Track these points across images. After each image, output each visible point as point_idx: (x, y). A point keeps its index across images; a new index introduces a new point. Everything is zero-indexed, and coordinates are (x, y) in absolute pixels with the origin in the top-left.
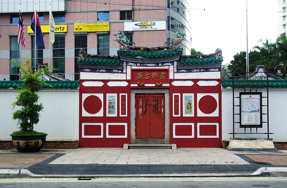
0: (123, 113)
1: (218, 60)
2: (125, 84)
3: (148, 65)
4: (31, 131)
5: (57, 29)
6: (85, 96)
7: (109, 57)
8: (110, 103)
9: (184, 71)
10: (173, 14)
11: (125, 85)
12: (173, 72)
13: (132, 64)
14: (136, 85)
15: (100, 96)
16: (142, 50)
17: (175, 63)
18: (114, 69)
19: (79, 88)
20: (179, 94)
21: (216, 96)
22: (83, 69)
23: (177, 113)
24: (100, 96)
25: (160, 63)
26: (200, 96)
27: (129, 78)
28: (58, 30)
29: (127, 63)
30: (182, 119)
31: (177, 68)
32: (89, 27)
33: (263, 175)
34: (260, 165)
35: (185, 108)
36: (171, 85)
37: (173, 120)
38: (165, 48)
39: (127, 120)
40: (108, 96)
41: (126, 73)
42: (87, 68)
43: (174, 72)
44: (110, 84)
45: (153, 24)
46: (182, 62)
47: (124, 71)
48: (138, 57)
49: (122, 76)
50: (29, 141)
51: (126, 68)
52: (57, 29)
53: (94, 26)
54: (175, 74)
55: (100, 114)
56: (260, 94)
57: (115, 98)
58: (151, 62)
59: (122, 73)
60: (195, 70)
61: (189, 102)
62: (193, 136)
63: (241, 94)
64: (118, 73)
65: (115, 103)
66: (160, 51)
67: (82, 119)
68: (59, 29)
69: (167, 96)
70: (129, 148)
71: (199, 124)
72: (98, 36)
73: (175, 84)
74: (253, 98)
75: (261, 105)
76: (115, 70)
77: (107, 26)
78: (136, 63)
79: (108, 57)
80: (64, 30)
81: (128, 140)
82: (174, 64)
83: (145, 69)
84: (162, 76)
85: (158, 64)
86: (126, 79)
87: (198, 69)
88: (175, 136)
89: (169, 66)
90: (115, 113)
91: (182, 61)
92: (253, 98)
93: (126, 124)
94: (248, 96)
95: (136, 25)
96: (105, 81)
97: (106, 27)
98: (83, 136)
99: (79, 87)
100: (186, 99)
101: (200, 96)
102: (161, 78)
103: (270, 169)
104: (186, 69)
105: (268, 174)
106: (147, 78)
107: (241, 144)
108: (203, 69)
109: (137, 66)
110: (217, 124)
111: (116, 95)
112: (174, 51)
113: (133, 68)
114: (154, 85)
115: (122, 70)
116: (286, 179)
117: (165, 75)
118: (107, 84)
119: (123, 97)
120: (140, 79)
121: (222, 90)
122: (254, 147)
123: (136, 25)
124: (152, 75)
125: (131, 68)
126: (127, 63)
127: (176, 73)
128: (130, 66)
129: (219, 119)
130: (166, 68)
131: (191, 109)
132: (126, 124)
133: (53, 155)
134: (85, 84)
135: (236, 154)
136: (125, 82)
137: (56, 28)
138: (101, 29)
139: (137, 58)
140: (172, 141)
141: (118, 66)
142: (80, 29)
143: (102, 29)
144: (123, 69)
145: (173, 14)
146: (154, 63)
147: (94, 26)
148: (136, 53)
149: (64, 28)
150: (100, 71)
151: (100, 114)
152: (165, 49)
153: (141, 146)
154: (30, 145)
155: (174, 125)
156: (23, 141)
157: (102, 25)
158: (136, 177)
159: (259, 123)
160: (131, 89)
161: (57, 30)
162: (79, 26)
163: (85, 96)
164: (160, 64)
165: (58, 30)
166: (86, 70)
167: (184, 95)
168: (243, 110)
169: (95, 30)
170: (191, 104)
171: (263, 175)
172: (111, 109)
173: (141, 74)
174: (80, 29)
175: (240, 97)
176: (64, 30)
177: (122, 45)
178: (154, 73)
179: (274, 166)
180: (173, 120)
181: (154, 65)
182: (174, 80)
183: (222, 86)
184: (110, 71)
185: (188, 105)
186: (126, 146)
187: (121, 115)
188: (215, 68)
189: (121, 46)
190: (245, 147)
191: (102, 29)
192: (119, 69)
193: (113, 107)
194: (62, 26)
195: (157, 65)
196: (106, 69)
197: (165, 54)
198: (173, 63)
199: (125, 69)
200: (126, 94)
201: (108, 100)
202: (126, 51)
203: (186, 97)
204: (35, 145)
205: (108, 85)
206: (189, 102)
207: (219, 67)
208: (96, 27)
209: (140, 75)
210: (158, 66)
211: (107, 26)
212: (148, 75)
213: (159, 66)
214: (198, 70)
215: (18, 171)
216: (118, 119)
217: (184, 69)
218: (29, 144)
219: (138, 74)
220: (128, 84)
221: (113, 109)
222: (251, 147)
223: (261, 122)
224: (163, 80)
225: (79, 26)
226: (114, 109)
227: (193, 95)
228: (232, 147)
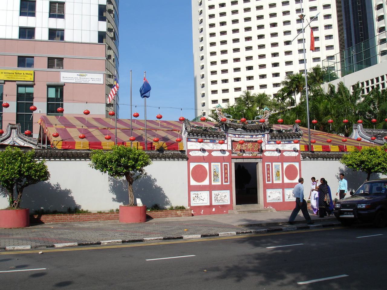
3: (246, 136)
6: (193, 165)
15: (206, 165)
24: (206, 165)
26: (286, 165)
27: (230, 148)
32: (7, 74)
41: (227, 144)
53: (14, 74)
61: (278, 170)
72: (19, 86)
73: (266, 154)
77: (31, 74)
90: (219, 182)
95: (77, 75)
97: (30, 75)
100: (275, 168)
101: (286, 165)
109: (236, 137)
113: (233, 139)
138: (23, 77)
143: (25, 77)
147: (14, 74)
163: (193, 165)
164: (254, 136)
166: (192, 140)
169: (15, 78)
172: (215, 178)
181: (249, 136)
187: (224, 184)
191: (25, 77)
193: (217, 175)
203: (275, 166)
206: (278, 170)
208: (16, 75)
211: (31, 74)
227: (280, 164)
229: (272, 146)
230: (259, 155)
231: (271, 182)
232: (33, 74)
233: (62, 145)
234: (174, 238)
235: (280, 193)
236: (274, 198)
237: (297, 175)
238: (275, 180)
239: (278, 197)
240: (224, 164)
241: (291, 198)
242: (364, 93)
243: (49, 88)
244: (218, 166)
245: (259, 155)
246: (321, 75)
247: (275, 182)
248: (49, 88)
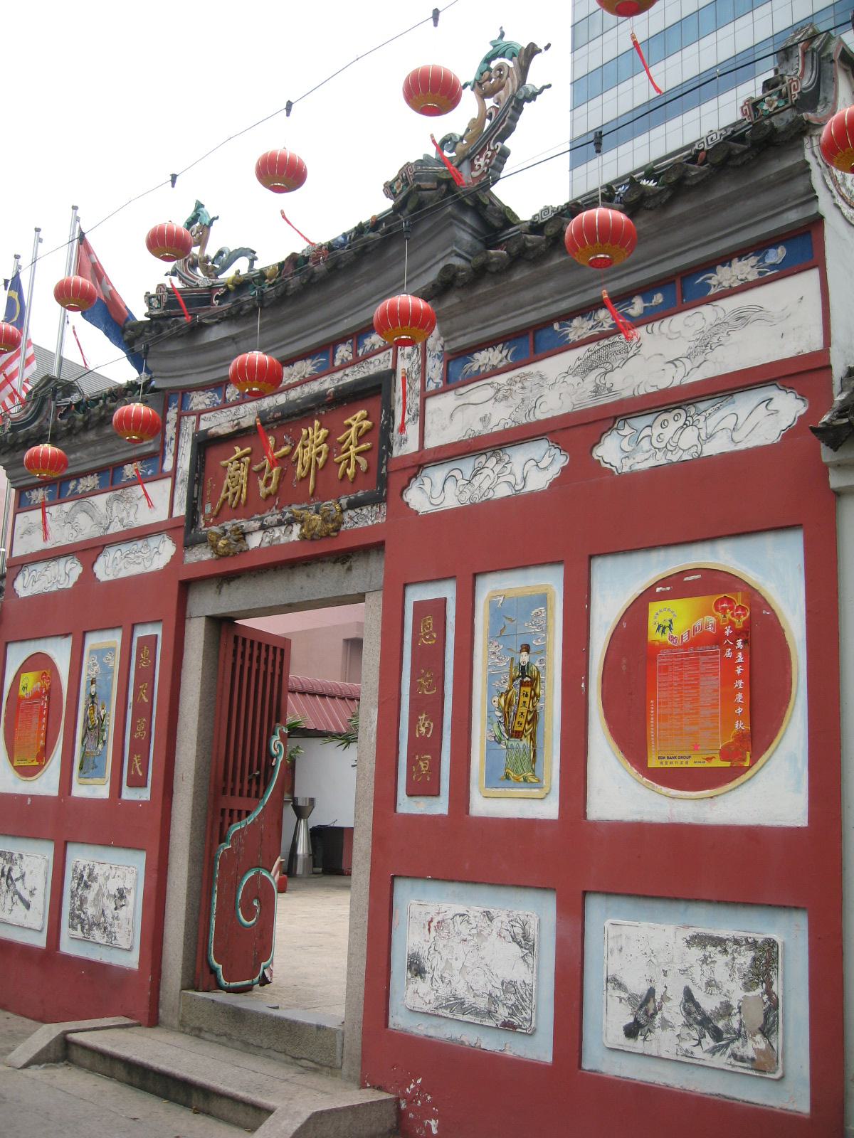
2: (160, 553)
8: (93, 697)
11: (69, 584)
35: (490, 723)
61: (524, 658)
100: (497, 634)
108: (645, 290)
139: (206, 341)
164: (344, 352)
206: (524, 658)
207: (792, 216)
229: (490, 392)
230: (368, 519)
231: (439, 806)
233: (61, 359)
235: (525, 942)
236: (462, 991)
238: (489, 784)
239: (509, 986)
241: (663, 1041)
245: (368, 519)
246: (283, 1128)
247: (482, 805)
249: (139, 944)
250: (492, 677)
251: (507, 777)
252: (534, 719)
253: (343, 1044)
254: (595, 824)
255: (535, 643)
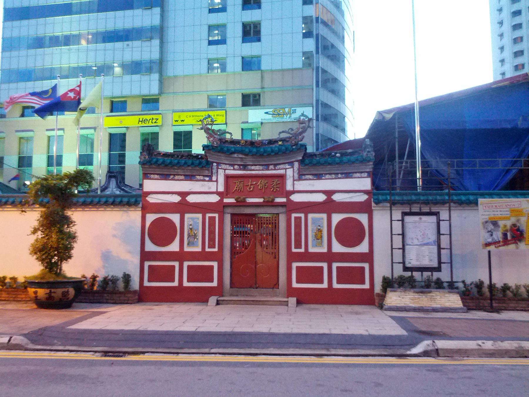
0: (212, 246)
1: (366, 159)
2: (215, 199)
3: (253, 168)
4: (59, 274)
5: (147, 121)
7: (190, 156)
8: (191, 229)
9: (311, 177)
10: (326, 97)
12: (292, 179)
13: (227, 167)
14: (232, 200)
16: (243, 144)
17: (296, 165)
18: (197, 175)
19: (140, 205)
20: (302, 215)
21: (363, 218)
22: (149, 175)
23: (298, 246)
24: (175, 218)
25: (271, 165)
26: (337, 218)
27: (221, 189)
28: (149, 123)
29: (218, 164)
30: (307, 256)
31: (299, 172)
33: (426, 354)
34: (422, 336)
36: (289, 200)
37: (292, 257)
38: (280, 141)
39: (218, 257)
40: (188, 218)
41: (217, 181)
42: (156, 173)
43: (293, 178)
44: (191, 199)
45: (293, 112)
46: (305, 162)
47: (214, 178)
48: (236, 155)
49: (211, 186)
50: (53, 290)
51: (217, 172)
52: (147, 122)
54: (295, 182)
55: (174, 247)
56: (437, 214)
57: (198, 221)
58: (256, 163)
59: (211, 180)
60: (328, 176)
61: (319, 228)
62: (325, 285)
63: (404, 214)
64: (204, 180)
65: (198, 229)
66: (271, 146)
67: (145, 256)
68: (151, 121)
69: (282, 220)
70: (218, 303)
71: (335, 265)
73: (296, 198)
74: (425, 222)
75: (439, 233)
76: (199, 175)
77: (223, 116)
78: (233, 165)
79: (188, 156)
80: (157, 123)
81: (218, 291)
82: (294, 167)
83: (286, 183)
84: (273, 186)
85: (268, 165)
86: (216, 191)
87: (334, 174)
88: (295, 285)
89: (286, 169)
90: (197, 246)
91: (307, 161)
92: (425, 222)
93: (215, 264)
94: (416, 218)
95: (266, 113)
96: (183, 195)
97: (222, 117)
98: (146, 284)
99: (141, 203)
101: (337, 218)
102: (273, 190)
103: (441, 344)
104: (312, 175)
105: (437, 353)
106: (250, 188)
107: (404, 299)
108: (342, 174)
109: (234, 169)
110: (366, 266)
111: (200, 216)
112: (294, 146)
113: (228, 172)
114: (261, 200)
115: (210, 177)
116: (528, 362)
117: (279, 183)
118: (187, 198)
119: (212, 219)
120: (238, 191)
121: (373, 208)
122: (427, 305)
123: (266, 113)
124: (259, 185)
125: (225, 172)
126: (218, 164)
127: (298, 180)
128: (224, 170)
129: (368, 257)
130: (282, 172)
131: (321, 240)
132: (215, 264)
133: (84, 313)
134: (151, 199)
135: (391, 317)
136: (216, 195)
137: (146, 120)
140: (291, 292)
141: (204, 170)
142: (181, 121)
144: (212, 175)
145: (326, 97)
146: (262, 165)
148: (233, 149)
149: (157, 119)
150: (175, 178)
151: (174, 247)
152: (280, 143)
153: (238, 300)
154: (53, 297)
155: (295, 265)
156: (43, 290)
157: (215, 115)
158: (202, 353)
159: (435, 264)
160: (224, 206)
161: (146, 123)
162: (179, 117)
163: (151, 218)
164: (271, 167)
165: (149, 123)
166: (152, 176)
167: (311, 216)
168: (408, 241)
170: (321, 231)
171: (426, 354)
172: (191, 239)
173: (240, 182)
174: (181, 121)
175: (403, 220)
176: (157, 123)
177: (212, 137)
178: (261, 181)
179: (450, 338)
180: (292, 257)
181: (261, 168)
182: (293, 192)
183: (373, 201)
184: (191, 178)
185: (317, 233)
186: (213, 300)
187: (207, 250)
188: (362, 172)
189: (210, 139)
190: (411, 305)
192: (204, 174)
193: (195, 236)
194: (155, 117)
195: (267, 168)
196: (184, 175)
197: (280, 150)
198: (291, 164)
199: (216, 174)
200: (216, 215)
201: (188, 225)
202: (215, 145)
203: (313, 219)
204: (62, 297)
205: (188, 200)
209: (237, 185)
210: (269, 170)
211: (223, 116)
212: (251, 185)
213: (270, 170)
214: (333, 175)
215: (7, 339)
216: (203, 256)
217: (310, 174)
218: (53, 295)
219: (236, 183)
220: (219, 198)
221: (195, 240)
222: (422, 305)
223: (440, 263)
224: (275, 192)
225: (179, 117)
226: (197, 239)
227: (324, 216)
228: (389, 305)
232: (225, 115)
234: (12, 211)
237: (335, 229)
240: (215, 217)
242: (104, 99)
243: (402, 264)
244: (198, 219)
248: (144, 180)
249: (162, 286)
250: (312, 230)
251: (316, 246)
252: (321, 237)
253: (77, 339)
254: (369, 251)
255: (321, 225)
